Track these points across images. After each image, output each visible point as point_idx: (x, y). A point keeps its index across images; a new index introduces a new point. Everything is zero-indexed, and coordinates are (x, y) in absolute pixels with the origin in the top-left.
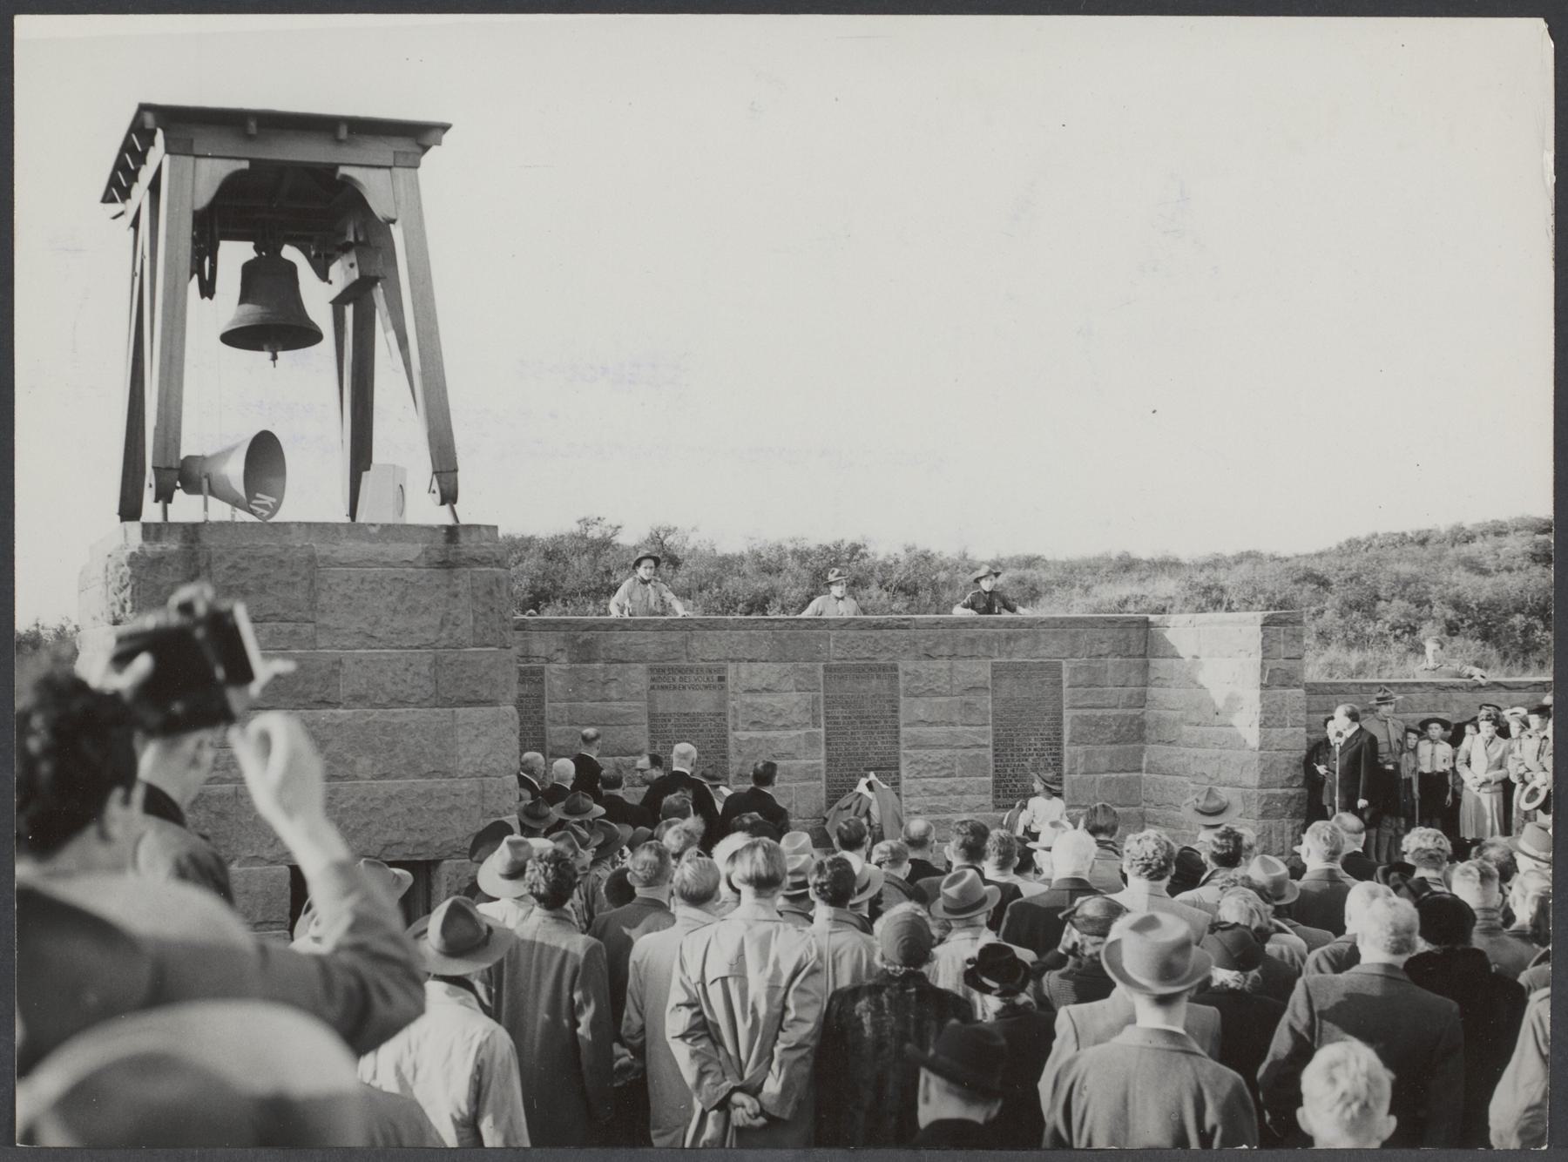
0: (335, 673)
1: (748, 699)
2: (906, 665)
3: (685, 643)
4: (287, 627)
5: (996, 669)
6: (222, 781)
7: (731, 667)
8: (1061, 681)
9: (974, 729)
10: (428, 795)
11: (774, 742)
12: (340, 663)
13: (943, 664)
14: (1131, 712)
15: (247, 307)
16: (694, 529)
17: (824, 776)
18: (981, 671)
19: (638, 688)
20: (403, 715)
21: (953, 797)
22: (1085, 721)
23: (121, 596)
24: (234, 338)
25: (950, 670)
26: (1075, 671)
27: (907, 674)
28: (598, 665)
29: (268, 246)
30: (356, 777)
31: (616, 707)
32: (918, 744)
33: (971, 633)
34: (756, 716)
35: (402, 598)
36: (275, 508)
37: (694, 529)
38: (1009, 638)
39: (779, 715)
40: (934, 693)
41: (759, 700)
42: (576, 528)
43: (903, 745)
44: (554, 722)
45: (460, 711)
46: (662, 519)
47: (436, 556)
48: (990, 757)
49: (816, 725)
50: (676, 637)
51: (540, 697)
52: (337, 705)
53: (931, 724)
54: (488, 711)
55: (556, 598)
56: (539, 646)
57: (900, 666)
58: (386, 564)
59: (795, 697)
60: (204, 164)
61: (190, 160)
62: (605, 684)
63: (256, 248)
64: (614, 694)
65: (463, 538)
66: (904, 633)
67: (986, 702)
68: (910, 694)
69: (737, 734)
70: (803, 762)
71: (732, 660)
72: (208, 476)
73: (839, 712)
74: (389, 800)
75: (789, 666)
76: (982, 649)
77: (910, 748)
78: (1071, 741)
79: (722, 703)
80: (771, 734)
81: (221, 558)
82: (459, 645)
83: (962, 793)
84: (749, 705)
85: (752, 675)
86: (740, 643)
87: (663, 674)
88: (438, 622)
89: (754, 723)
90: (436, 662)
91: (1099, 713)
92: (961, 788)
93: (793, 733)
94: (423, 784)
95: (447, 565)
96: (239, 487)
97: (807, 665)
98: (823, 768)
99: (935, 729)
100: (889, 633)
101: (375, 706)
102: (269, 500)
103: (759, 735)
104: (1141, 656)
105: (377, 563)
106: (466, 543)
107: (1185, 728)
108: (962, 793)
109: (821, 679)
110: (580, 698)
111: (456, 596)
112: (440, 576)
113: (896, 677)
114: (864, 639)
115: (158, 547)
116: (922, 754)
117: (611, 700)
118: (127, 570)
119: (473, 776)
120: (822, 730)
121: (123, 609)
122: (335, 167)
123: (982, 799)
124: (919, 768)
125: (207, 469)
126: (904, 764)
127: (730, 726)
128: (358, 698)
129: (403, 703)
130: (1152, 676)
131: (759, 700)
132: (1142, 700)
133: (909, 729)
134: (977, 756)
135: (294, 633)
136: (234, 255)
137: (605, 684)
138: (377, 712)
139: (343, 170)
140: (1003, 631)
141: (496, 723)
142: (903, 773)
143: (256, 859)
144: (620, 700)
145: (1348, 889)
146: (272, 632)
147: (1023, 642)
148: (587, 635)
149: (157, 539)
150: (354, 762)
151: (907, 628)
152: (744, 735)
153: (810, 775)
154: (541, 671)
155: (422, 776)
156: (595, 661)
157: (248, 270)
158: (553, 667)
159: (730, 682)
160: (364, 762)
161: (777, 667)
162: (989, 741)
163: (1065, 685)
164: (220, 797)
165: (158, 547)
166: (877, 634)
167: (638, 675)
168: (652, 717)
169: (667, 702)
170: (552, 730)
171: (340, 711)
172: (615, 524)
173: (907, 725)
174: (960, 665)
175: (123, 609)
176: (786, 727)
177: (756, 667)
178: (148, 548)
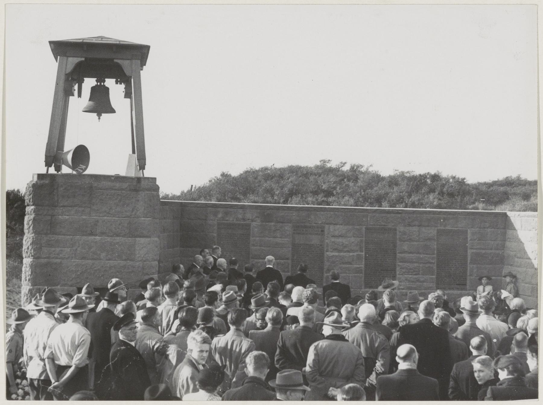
0: (96, 225)
1: (333, 240)
2: (401, 228)
4: (80, 209)
5: (438, 231)
6: (57, 258)
7: (327, 226)
8: (467, 238)
9: (428, 256)
12: (98, 221)
13: (415, 229)
15: (91, 103)
16: (371, 166)
17: (363, 272)
18: (432, 232)
20: (118, 239)
24: (89, 110)
25: (419, 231)
27: (400, 232)
28: (273, 224)
29: (101, 80)
30: (101, 259)
31: (279, 240)
32: (403, 261)
35: (120, 201)
36: (86, 169)
37: (371, 166)
39: (345, 247)
41: (338, 240)
42: (319, 164)
43: (398, 261)
44: (254, 245)
45: (138, 239)
48: (435, 268)
52: (96, 235)
53: (411, 253)
54: (149, 239)
55: (299, 194)
57: (398, 229)
58: (115, 190)
59: (353, 239)
60: (70, 59)
61: (65, 58)
62: (275, 231)
63: (96, 81)
65: (143, 182)
66: (399, 215)
68: (401, 240)
69: (328, 253)
70: (355, 266)
71: (327, 224)
72: (62, 159)
74: (111, 267)
75: (350, 227)
77: (400, 262)
78: (470, 263)
80: (342, 254)
81: (62, 186)
82: (138, 217)
84: (333, 242)
85: (335, 230)
88: (131, 209)
89: (336, 249)
91: (483, 251)
92: (422, 279)
93: (351, 254)
94: (122, 263)
96: (70, 162)
97: (358, 227)
98: (363, 269)
99: (411, 255)
100: (393, 215)
101: (108, 236)
102: (84, 167)
103: (337, 254)
104: (503, 229)
105: (113, 189)
106: (143, 184)
107: (516, 259)
108: (423, 282)
109: (364, 232)
111: (138, 201)
113: (396, 233)
114: (382, 217)
115: (42, 182)
116: (406, 265)
117: (277, 237)
118: (31, 189)
119: (140, 261)
120: (363, 253)
122: (113, 59)
123: (431, 285)
124: (404, 270)
125: (63, 156)
126: (398, 269)
128: (102, 234)
129: (118, 236)
130: (507, 237)
131: (338, 240)
132: (503, 247)
133: (400, 255)
134: (429, 267)
135: (83, 211)
136: (89, 83)
137: (275, 231)
139: (115, 61)
141: (149, 244)
142: (398, 273)
143: (65, 285)
144: (281, 238)
145: (463, 318)
146: (76, 210)
148: (269, 212)
149: (42, 179)
150: (100, 254)
151: (400, 213)
152: (330, 254)
153: (358, 271)
154: (249, 225)
155: (123, 260)
156: (271, 222)
157: (93, 89)
158: (254, 224)
159: (326, 232)
160: (103, 255)
161: (346, 227)
162: (435, 261)
163: (469, 239)
164: (56, 263)
165: (42, 182)
166: (389, 215)
167: (288, 228)
171: (97, 237)
172: (344, 162)
173: (399, 253)
175: (30, 201)
176: (348, 251)
178: (39, 182)
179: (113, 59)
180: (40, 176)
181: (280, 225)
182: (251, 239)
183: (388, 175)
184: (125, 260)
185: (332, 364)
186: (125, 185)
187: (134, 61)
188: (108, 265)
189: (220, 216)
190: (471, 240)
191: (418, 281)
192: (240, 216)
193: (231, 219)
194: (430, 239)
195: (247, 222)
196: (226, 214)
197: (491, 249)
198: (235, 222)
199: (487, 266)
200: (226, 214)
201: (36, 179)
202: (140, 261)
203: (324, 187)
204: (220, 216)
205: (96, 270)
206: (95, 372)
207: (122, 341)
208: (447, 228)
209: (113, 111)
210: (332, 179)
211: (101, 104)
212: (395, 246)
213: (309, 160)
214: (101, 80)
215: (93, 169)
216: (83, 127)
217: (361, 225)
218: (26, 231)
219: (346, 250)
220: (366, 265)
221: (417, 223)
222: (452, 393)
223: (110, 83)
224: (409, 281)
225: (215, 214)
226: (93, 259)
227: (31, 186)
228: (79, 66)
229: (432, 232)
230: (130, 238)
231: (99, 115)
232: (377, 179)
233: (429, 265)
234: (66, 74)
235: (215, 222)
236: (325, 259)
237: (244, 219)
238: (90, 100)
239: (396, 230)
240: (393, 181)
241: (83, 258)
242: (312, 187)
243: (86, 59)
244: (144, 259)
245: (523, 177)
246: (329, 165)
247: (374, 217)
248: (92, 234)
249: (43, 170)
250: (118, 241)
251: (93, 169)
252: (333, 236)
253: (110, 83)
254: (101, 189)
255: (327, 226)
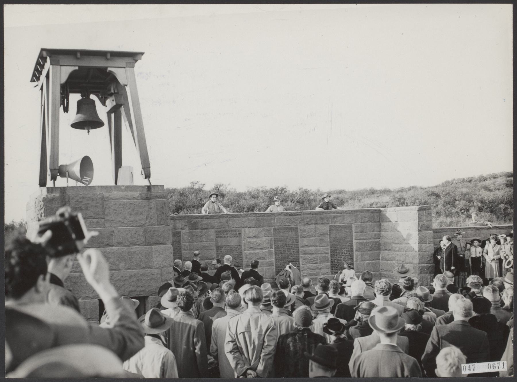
0: (112, 235)
1: (249, 240)
2: (301, 227)
3: (227, 222)
5: (330, 228)
7: (243, 230)
9: (324, 247)
10: (143, 275)
11: (258, 254)
13: (312, 226)
14: (376, 240)
17: (274, 265)
18: (325, 228)
19: (212, 237)
20: (134, 248)
21: (318, 270)
22: (361, 244)
23: (41, 212)
24: (76, 125)
25: (315, 228)
26: (357, 227)
27: (301, 230)
28: (198, 230)
29: (85, 95)
30: (120, 269)
31: (205, 244)
33: (322, 216)
34: (251, 245)
35: (133, 210)
36: (90, 182)
37: (229, 184)
38: (334, 217)
40: (310, 236)
43: (300, 254)
44: (185, 249)
46: (218, 182)
47: (144, 196)
49: (271, 248)
50: (224, 220)
51: (180, 241)
52: (113, 246)
54: (164, 246)
56: (179, 225)
58: (128, 199)
59: (264, 239)
60: (63, 68)
61: (59, 67)
63: (81, 96)
64: (204, 240)
65: (153, 190)
66: (299, 216)
67: (327, 239)
70: (267, 260)
71: (243, 227)
72: (68, 171)
73: (279, 243)
74: (131, 277)
75: (262, 229)
76: (326, 221)
77: (303, 254)
78: (356, 251)
79: (240, 242)
80: (256, 251)
81: (73, 198)
82: (153, 225)
83: (320, 269)
84: (249, 242)
85: (250, 232)
86: (245, 222)
87: (220, 233)
89: (251, 248)
90: (145, 231)
91: (365, 241)
92: (320, 267)
93: (264, 251)
94: (142, 271)
95: (148, 199)
96: (78, 174)
97: (268, 228)
98: (274, 262)
99: (310, 248)
100: (294, 217)
101: (125, 246)
102: (88, 179)
103: (253, 252)
107: (394, 245)
108: (320, 269)
110: (193, 241)
112: (145, 202)
113: (298, 231)
115: (52, 195)
117: (203, 242)
118: (42, 203)
119: (158, 268)
120: (273, 249)
121: (41, 216)
122: (107, 68)
123: (327, 271)
126: (301, 260)
127: (243, 249)
128: (119, 243)
129: (134, 244)
130: (382, 228)
132: (379, 236)
134: (325, 256)
135: (98, 222)
138: (126, 248)
139: (109, 69)
140: (333, 215)
142: (301, 263)
144: (206, 241)
145: (449, 296)
146: (90, 222)
147: (339, 218)
148: (195, 221)
149: (52, 192)
150: (119, 265)
151: (300, 215)
153: (270, 264)
154: (180, 233)
156: (198, 229)
159: (242, 235)
160: (122, 265)
161: (259, 229)
162: (329, 251)
163: (353, 232)
164: (75, 277)
165: (52, 195)
166: (291, 217)
167: (212, 233)
168: (217, 247)
169: (222, 242)
170: (184, 252)
171: (114, 248)
172: (203, 184)
174: (318, 226)
175: (41, 216)
176: (261, 249)
177: (251, 229)
179: (107, 68)
182: (182, 244)
184: (144, 268)
187: (127, 69)
188: (128, 274)
191: (317, 268)
194: (323, 234)
197: (370, 239)
199: (368, 252)
202: (158, 268)
205: (117, 280)
208: (336, 224)
212: (298, 242)
217: (269, 227)
220: (276, 259)
221: (313, 222)
224: (311, 269)
227: (41, 200)
229: (325, 228)
230: (146, 247)
233: (325, 255)
239: (297, 228)
243: (79, 67)
244: (162, 266)
247: (280, 219)
250: (135, 250)
254: (113, 199)
255: (243, 230)
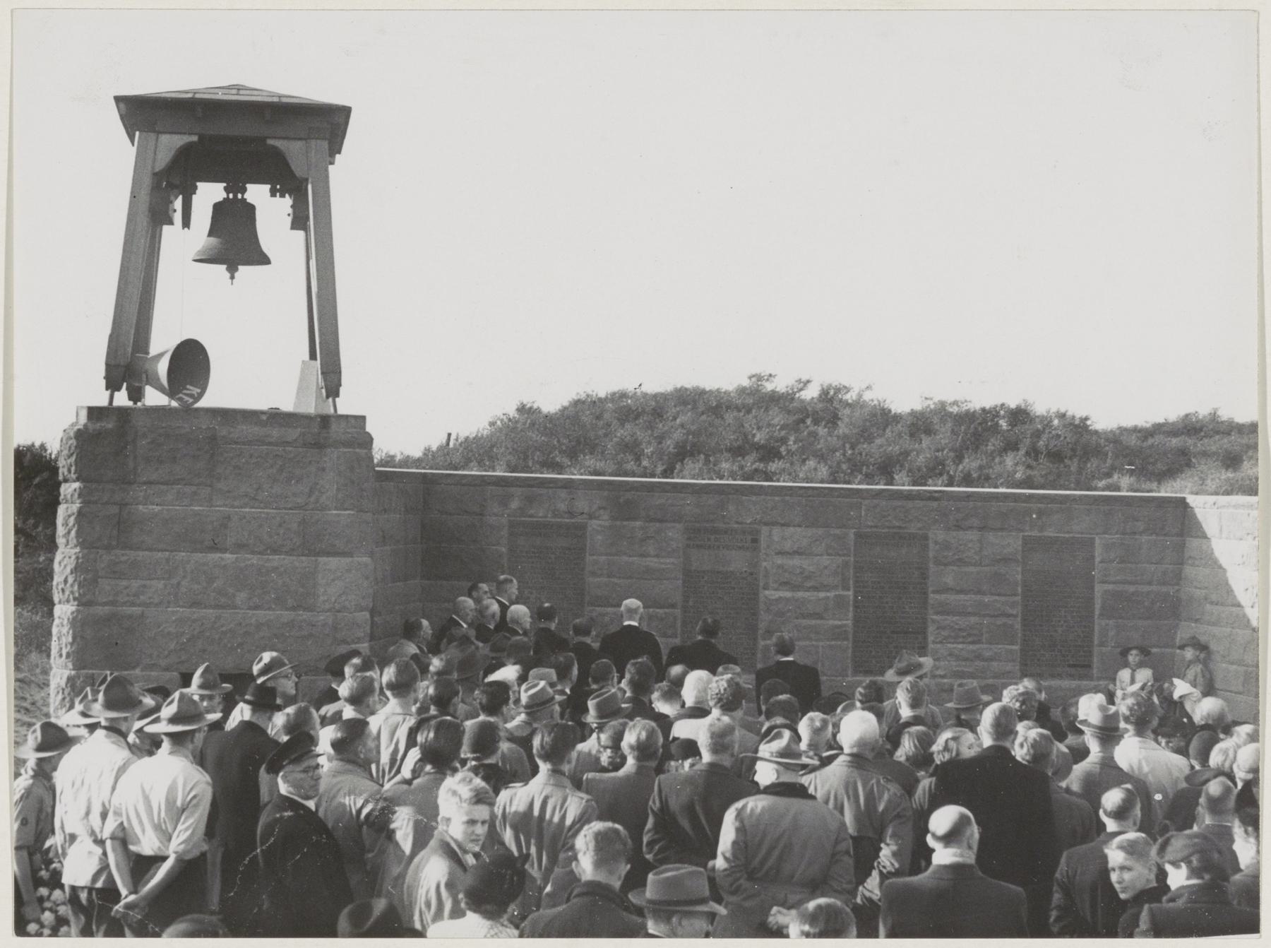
0: (226, 527)
1: (779, 561)
2: (938, 534)
4: (188, 489)
5: (1026, 541)
6: (133, 604)
7: (765, 530)
8: (1093, 557)
9: (1003, 599)
12: (229, 518)
13: (972, 535)
15: (213, 240)
16: (868, 388)
17: (851, 636)
18: (1011, 543)
20: (276, 560)
24: (209, 258)
25: (980, 541)
27: (936, 543)
28: (638, 523)
29: (236, 186)
30: (235, 607)
31: (652, 562)
32: (944, 610)
35: (281, 470)
36: (201, 395)
37: (868, 388)
39: (808, 578)
41: (791, 562)
42: (746, 383)
43: (931, 611)
44: (593, 574)
45: (322, 559)
48: (1018, 626)
52: (225, 551)
53: (961, 592)
54: (348, 560)
55: (699, 453)
57: (931, 535)
58: (270, 444)
59: (825, 561)
60: (164, 138)
61: (153, 136)
62: (643, 540)
63: (226, 189)
65: (334, 427)
66: (935, 504)
68: (938, 562)
69: (767, 592)
70: (831, 622)
71: (766, 524)
72: (146, 372)
74: (259, 626)
75: (820, 531)
77: (937, 613)
78: (1101, 615)
80: (800, 594)
81: (144, 436)
82: (324, 508)
84: (780, 567)
85: (784, 538)
88: (307, 490)
89: (786, 583)
91: (1132, 589)
92: (987, 654)
93: (822, 595)
94: (287, 615)
96: (164, 379)
97: (837, 531)
98: (850, 630)
99: (962, 596)
100: (919, 503)
101: (253, 553)
102: (196, 391)
103: (788, 594)
104: (1177, 535)
105: (264, 443)
106: (336, 430)
107: (1208, 607)
108: (991, 659)
109: (852, 543)
111: (324, 469)
113: (926, 546)
114: (895, 509)
115: (98, 426)
116: (950, 619)
117: (649, 556)
118: (73, 442)
119: (329, 610)
120: (851, 593)
122: (264, 139)
123: (1009, 667)
124: (945, 633)
125: (147, 366)
126: (931, 629)
128: (240, 547)
129: (275, 551)
130: (1187, 555)
131: (791, 562)
132: (1178, 578)
133: (937, 596)
134: (1005, 625)
135: (195, 493)
136: (209, 194)
137: (643, 540)
139: (270, 142)
141: (349, 571)
142: (931, 638)
143: (152, 667)
144: (657, 556)
145: (1084, 743)
146: (178, 492)
148: (629, 495)
149: (99, 419)
150: (234, 596)
151: (936, 499)
152: (772, 594)
153: (838, 634)
154: (583, 527)
155: (287, 609)
156: (635, 519)
157: (218, 208)
158: (594, 524)
159: (763, 544)
160: (241, 597)
161: (810, 532)
162: (1017, 611)
163: (1097, 560)
164: (130, 617)
165: (98, 426)
166: (910, 504)
167: (674, 534)
171: (227, 555)
172: (804, 379)
173: (934, 592)
175: (69, 471)
176: (815, 589)
178: (91, 426)
179: (264, 139)
180: (94, 413)
181: (655, 526)
182: (589, 558)
183: (907, 410)
184: (294, 608)
185: (776, 853)
186: (293, 434)
187: (313, 142)
188: (253, 621)
189: (514, 505)
190: (1101, 562)
191: (979, 657)
192: (562, 507)
193: (540, 513)
194: (1006, 560)
195: (579, 520)
196: (530, 500)
197: (1150, 583)
198: (550, 519)
199: (1140, 623)
200: (530, 500)
201: (83, 418)
202: (329, 610)
203: (759, 437)
204: (514, 505)
205: (224, 633)
206: (223, 871)
207: (287, 798)
208: (1046, 534)
209: (265, 260)
210: (778, 418)
211: (235, 243)
212: (924, 576)
213: (722, 374)
214: (236, 186)
215: (218, 394)
216: (193, 298)
217: (844, 526)
218: (60, 541)
219: (809, 584)
220: (857, 620)
221: (975, 522)
222: (1058, 919)
223: (257, 194)
224: (958, 658)
225: (504, 502)
226: (217, 607)
227: (72, 434)
228: (184, 154)
229: (1011, 543)
230: (304, 558)
231: (232, 270)
232: (882, 418)
233: (1004, 620)
234: (155, 174)
235: (504, 521)
236: (762, 606)
237: (571, 514)
238: (211, 234)
239: (926, 538)
240: (920, 424)
241: (195, 604)
242: (730, 438)
243: (201, 137)
244: (337, 606)
245: (1225, 414)
246: (769, 387)
247: (875, 507)
248: (215, 548)
249: (101, 399)
250: (276, 564)
251: (218, 394)
252: (780, 553)
253: (257, 194)
254: (236, 443)
255: (765, 530)
